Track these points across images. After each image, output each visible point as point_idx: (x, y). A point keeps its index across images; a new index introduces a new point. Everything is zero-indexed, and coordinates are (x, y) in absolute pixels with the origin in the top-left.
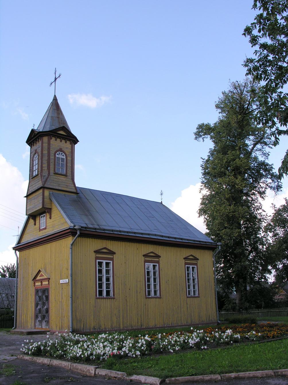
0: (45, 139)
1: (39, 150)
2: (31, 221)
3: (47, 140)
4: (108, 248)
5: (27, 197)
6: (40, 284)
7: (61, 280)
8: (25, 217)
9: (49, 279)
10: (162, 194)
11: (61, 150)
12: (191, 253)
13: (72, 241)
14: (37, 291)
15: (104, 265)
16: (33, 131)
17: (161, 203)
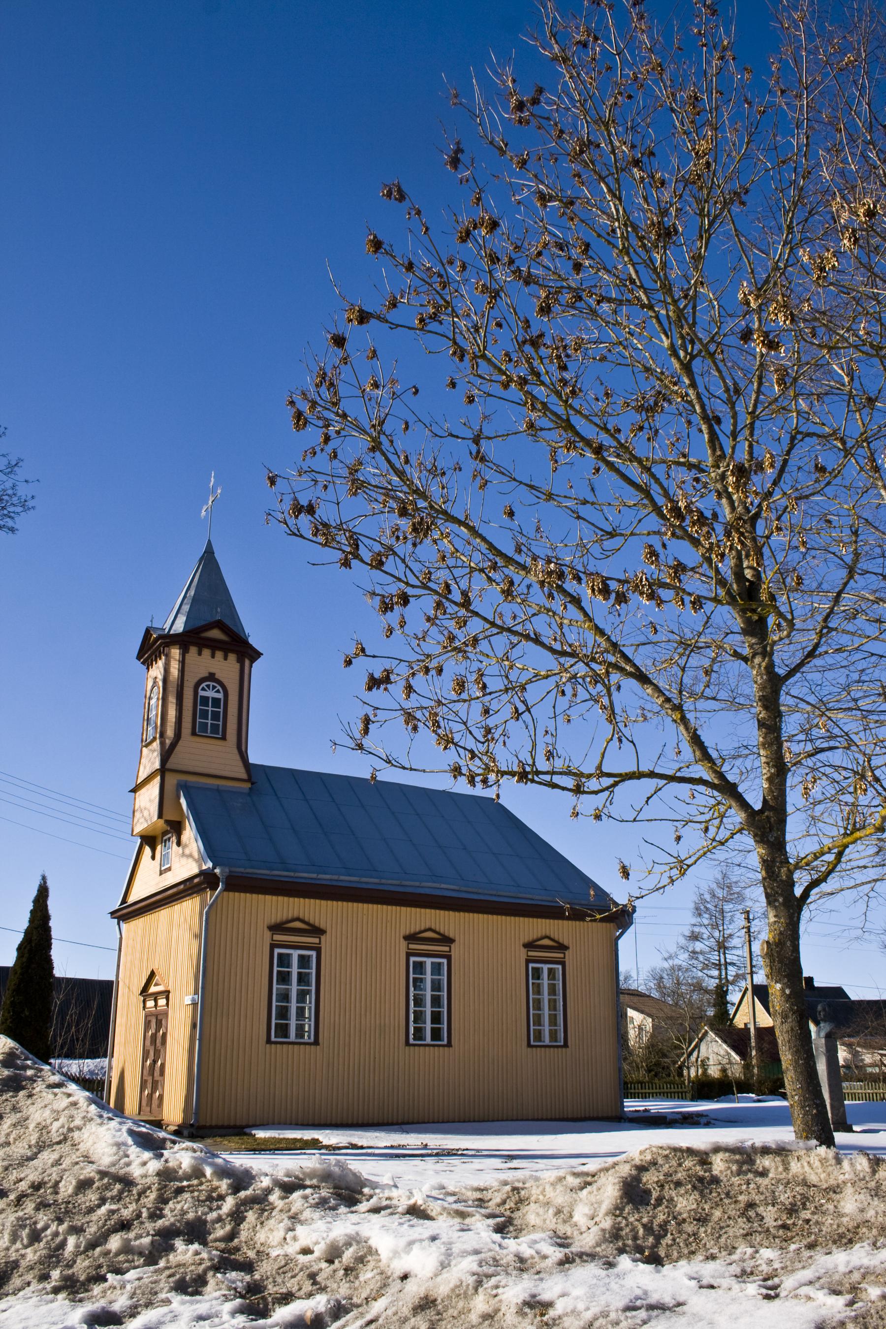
9: (169, 992)
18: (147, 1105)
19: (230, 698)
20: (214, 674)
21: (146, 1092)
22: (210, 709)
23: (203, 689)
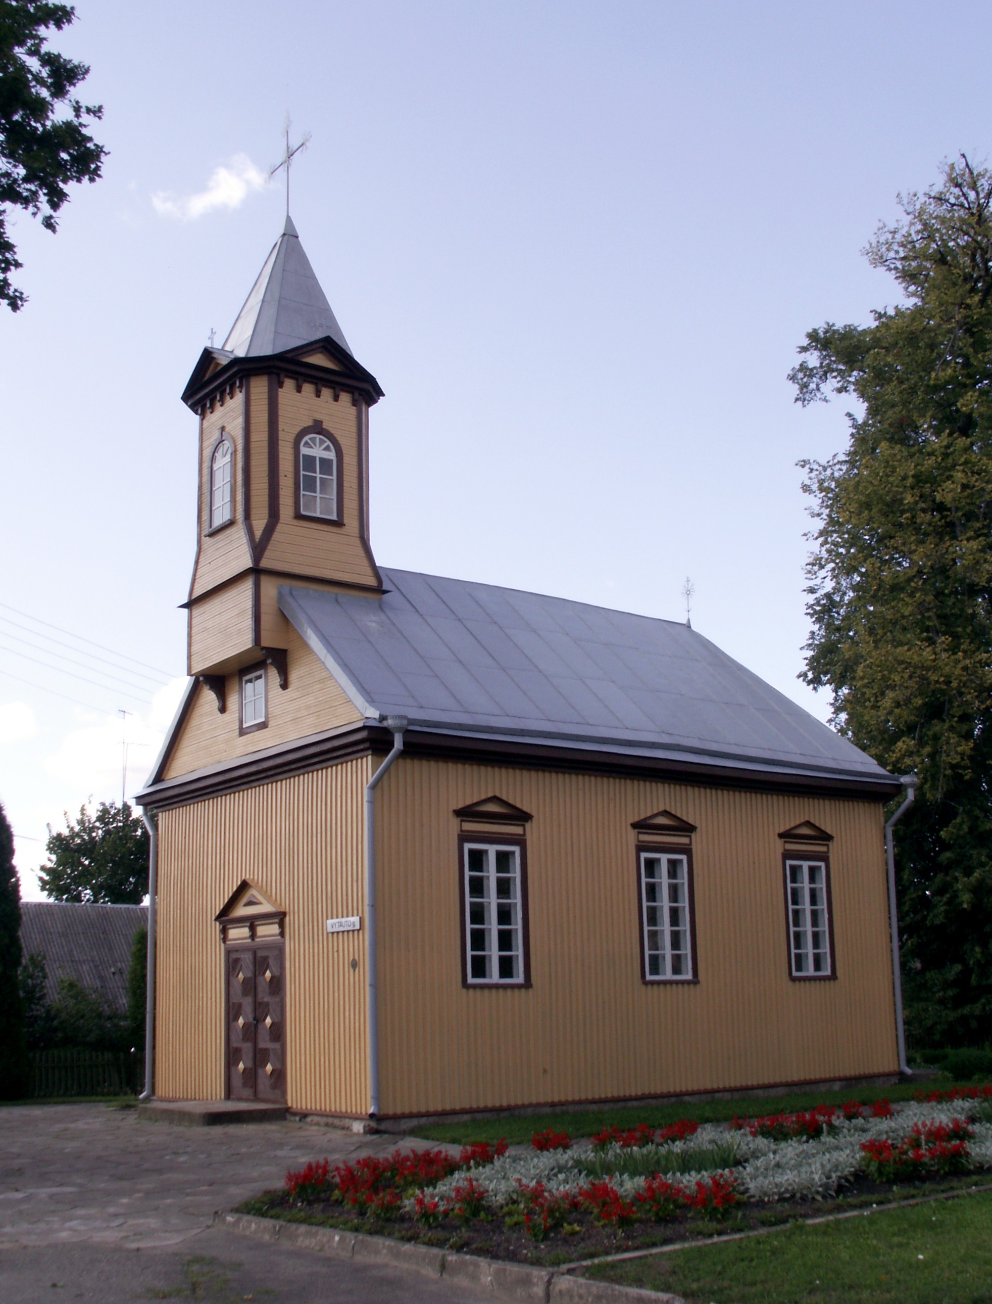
0: (259, 386)
1: (236, 426)
2: (209, 697)
3: (266, 389)
4: (504, 798)
5: (190, 605)
6: (244, 932)
7: (332, 918)
8: (184, 683)
9: (284, 914)
10: (688, 593)
11: (317, 428)
12: (668, 804)
13: (372, 775)
14: (232, 965)
15: (664, 867)
16: (207, 356)
17: (688, 626)
18: (245, 1085)
19: (346, 459)
20: (321, 422)
21: (241, 1066)
22: (318, 475)
23: (306, 444)
